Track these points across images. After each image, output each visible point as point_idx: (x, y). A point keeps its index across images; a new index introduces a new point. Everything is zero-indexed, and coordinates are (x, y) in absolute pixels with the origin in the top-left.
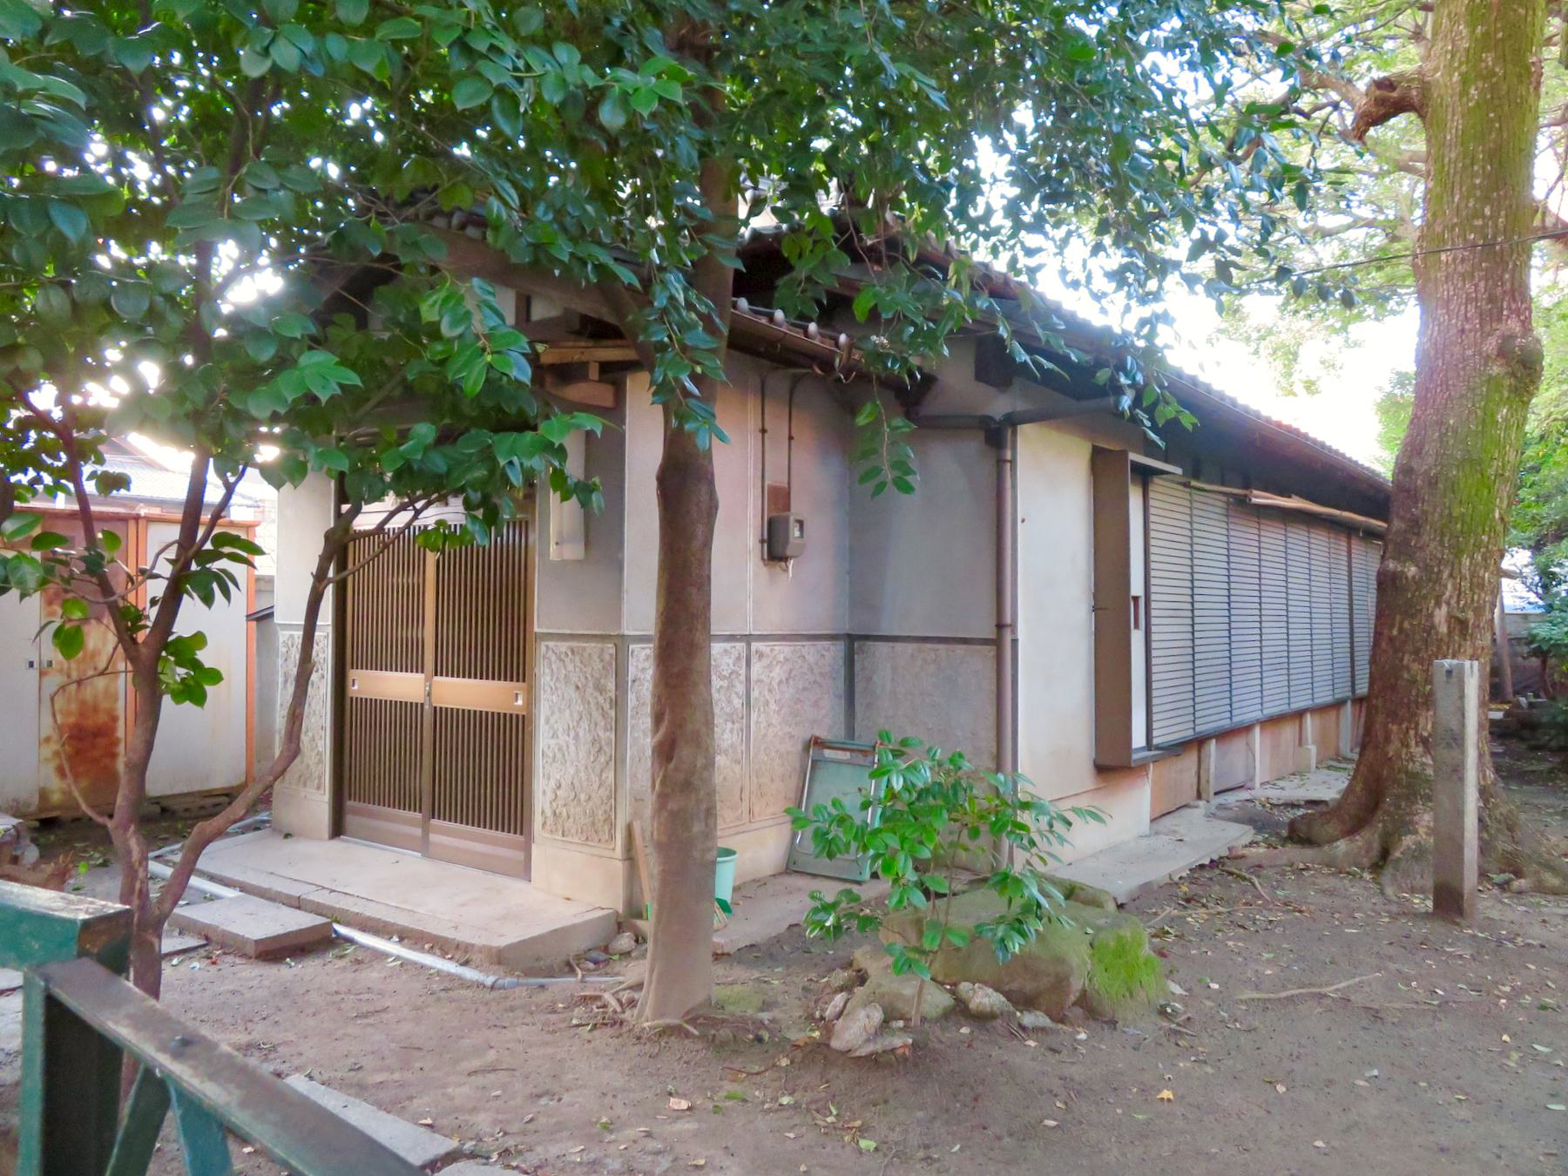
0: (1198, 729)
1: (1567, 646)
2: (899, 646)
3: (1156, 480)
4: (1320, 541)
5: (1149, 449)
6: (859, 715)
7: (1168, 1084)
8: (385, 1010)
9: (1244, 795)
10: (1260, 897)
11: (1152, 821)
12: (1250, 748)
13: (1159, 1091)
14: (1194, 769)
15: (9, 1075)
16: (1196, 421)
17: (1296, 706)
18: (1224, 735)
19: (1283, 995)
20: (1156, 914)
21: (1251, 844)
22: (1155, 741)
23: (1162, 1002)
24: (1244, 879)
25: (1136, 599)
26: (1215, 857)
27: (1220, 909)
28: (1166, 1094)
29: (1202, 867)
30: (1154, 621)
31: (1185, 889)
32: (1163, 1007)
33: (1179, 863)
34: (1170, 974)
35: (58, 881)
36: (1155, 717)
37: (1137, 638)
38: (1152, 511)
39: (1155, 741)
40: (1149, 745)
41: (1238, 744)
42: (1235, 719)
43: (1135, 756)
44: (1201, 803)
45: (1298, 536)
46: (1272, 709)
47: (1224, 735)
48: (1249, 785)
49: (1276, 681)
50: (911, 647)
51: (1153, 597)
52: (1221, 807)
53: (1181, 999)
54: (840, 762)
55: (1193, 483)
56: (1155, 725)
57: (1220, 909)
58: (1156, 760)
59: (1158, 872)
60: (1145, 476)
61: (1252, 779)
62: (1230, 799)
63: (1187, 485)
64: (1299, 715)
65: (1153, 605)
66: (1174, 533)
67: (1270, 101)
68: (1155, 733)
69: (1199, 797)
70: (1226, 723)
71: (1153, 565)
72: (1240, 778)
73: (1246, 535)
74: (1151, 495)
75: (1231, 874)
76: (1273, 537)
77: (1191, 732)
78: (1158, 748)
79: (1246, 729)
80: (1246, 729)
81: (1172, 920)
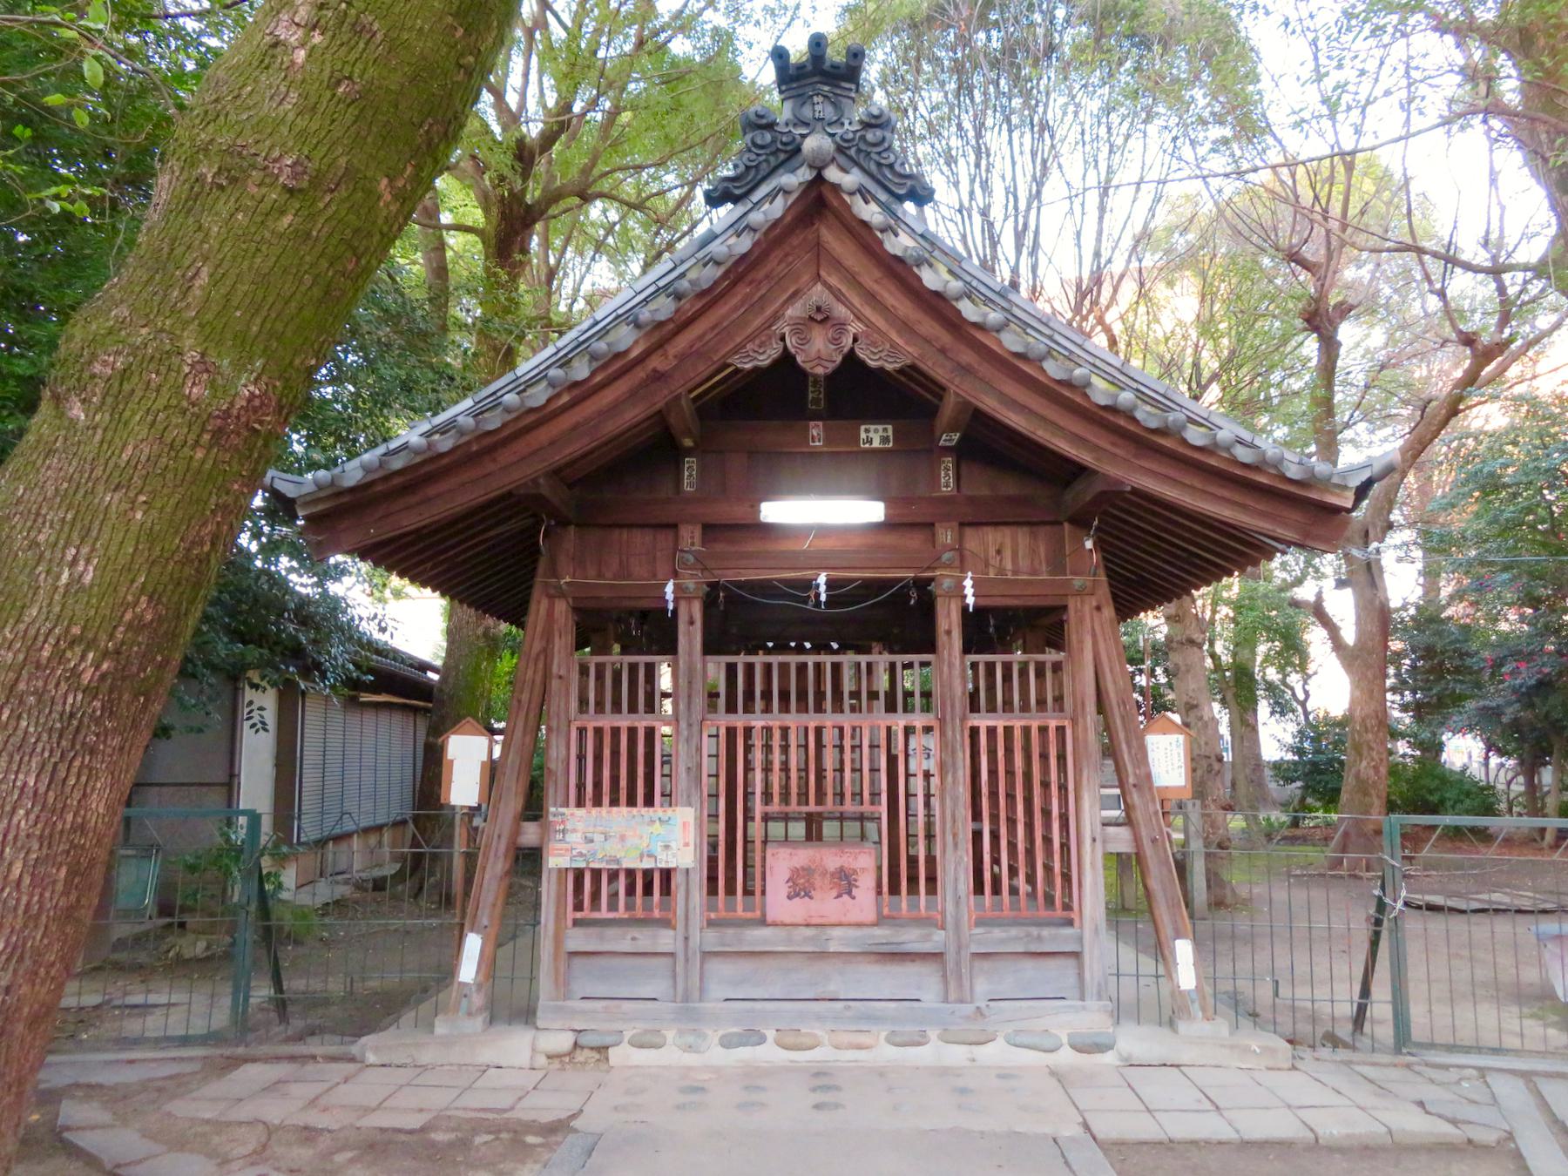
1: (1504, 2)
2: (164, 790)
4: (397, 718)
6: (133, 831)
11: (297, 888)
12: (350, 847)
17: (379, 822)
18: (338, 839)
35: (1217, 722)
41: (344, 846)
45: (384, 717)
46: (364, 823)
47: (338, 839)
49: (367, 805)
50: (172, 789)
54: (128, 856)
64: (379, 828)
66: (324, 725)
67: (445, 644)
73: (354, 719)
76: (369, 718)
79: (345, 837)
80: (345, 837)
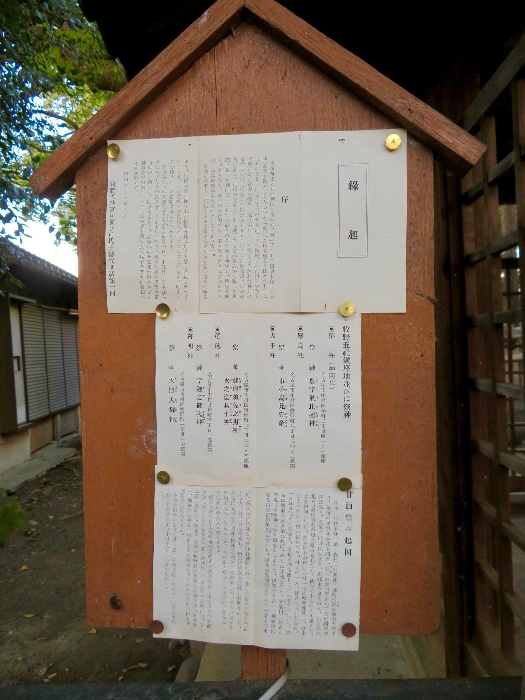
0: (52, 411)
3: (25, 305)
5: (20, 292)
7: (24, 563)
8: (233, 519)
9: (74, 435)
10: (76, 476)
11: (32, 453)
13: (21, 567)
14: (51, 428)
15: (524, 527)
16: (23, 285)
18: (63, 412)
19: (78, 514)
20: (29, 493)
21: (75, 455)
22: (31, 419)
23: (26, 530)
24: (70, 470)
25: (18, 358)
26: (58, 464)
27: (58, 485)
28: (24, 567)
29: (53, 469)
30: (27, 367)
31: (44, 480)
32: (27, 532)
33: (40, 468)
34: (32, 518)
36: (30, 408)
37: (18, 377)
38: (23, 318)
39: (31, 419)
40: (28, 420)
41: (70, 416)
42: (69, 405)
43: (19, 427)
44: (55, 442)
48: (77, 431)
51: (26, 356)
52: (64, 442)
53: (36, 526)
55: (43, 306)
56: (30, 412)
57: (58, 485)
58: (30, 427)
59: (31, 476)
60: (19, 305)
61: (78, 428)
62: (68, 438)
63: (40, 307)
65: (26, 360)
68: (30, 415)
69: (54, 439)
70: (64, 407)
71: (25, 342)
72: (73, 428)
74: (23, 312)
75: (65, 469)
77: (48, 413)
78: (32, 421)
81: (36, 494)
